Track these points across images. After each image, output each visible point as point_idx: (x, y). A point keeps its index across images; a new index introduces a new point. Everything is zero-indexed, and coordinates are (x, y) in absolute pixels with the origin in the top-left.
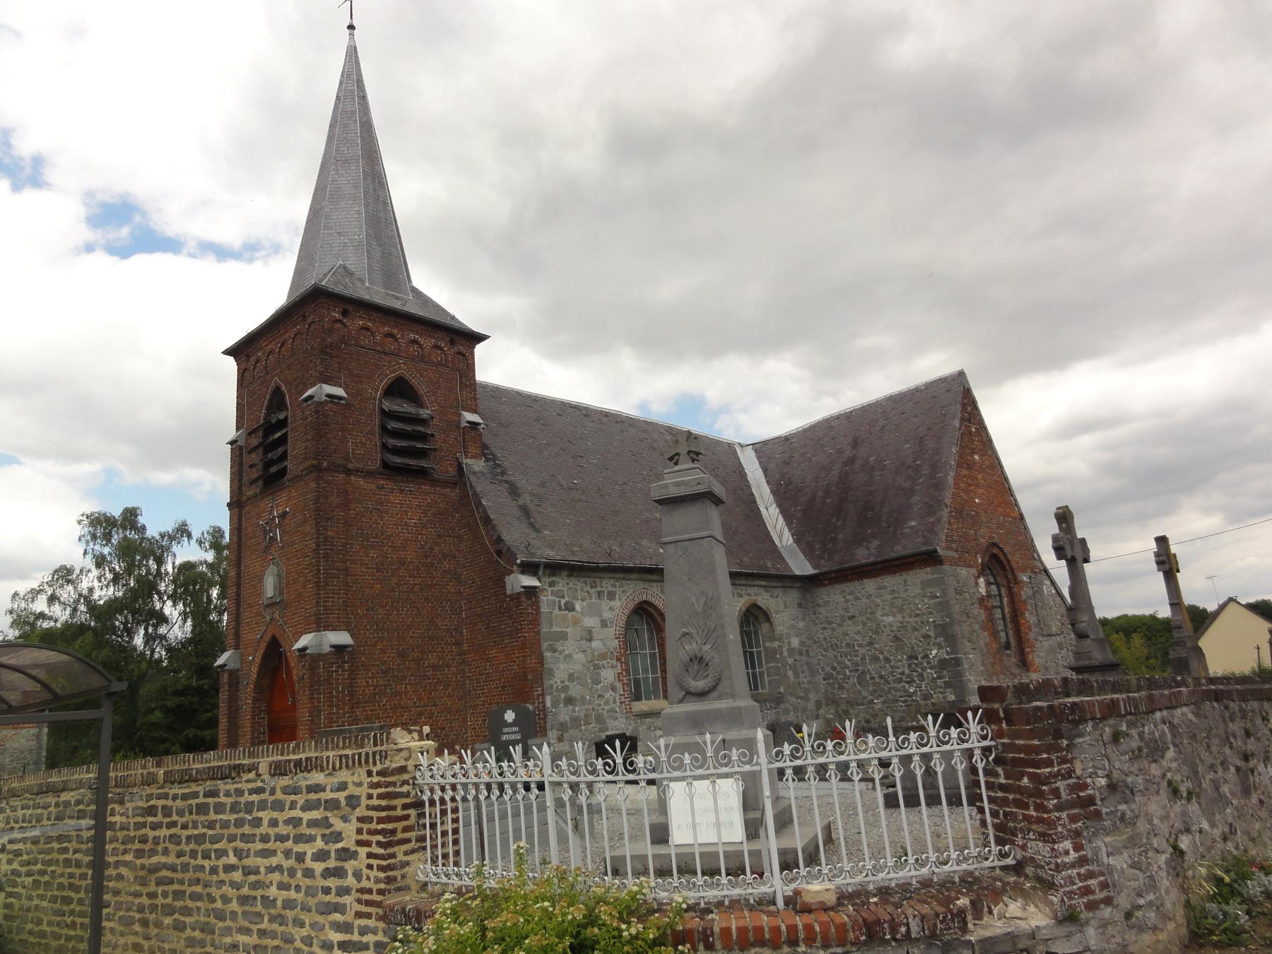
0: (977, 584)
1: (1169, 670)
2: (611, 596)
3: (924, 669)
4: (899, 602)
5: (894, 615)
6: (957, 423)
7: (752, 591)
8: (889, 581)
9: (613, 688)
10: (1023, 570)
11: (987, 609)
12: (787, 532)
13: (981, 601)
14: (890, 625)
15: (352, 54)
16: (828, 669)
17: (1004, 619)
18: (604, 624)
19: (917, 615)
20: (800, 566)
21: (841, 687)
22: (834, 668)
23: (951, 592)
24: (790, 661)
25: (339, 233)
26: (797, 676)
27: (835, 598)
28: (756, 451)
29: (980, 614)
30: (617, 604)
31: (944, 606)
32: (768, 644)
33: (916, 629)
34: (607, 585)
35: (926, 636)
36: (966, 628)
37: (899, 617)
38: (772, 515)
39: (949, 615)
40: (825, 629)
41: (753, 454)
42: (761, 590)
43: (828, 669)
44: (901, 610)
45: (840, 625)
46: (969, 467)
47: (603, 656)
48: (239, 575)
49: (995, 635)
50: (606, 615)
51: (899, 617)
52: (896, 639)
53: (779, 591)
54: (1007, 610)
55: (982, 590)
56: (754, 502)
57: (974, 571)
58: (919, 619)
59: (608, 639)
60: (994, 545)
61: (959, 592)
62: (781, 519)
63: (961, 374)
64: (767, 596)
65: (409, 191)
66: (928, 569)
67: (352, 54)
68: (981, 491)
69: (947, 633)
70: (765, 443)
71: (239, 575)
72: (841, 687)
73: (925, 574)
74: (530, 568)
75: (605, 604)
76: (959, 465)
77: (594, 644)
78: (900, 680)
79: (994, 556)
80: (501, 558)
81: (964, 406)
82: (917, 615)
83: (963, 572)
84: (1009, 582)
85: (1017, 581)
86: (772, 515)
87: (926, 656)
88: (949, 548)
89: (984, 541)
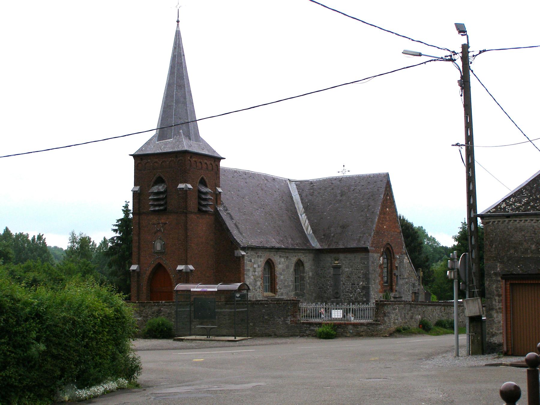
0: (380, 259)
1: (13, 331)
2: (261, 257)
3: (357, 289)
4: (351, 264)
5: (349, 268)
6: (382, 196)
7: (299, 254)
8: (349, 256)
9: (259, 288)
10: (398, 254)
11: (382, 269)
12: (309, 228)
13: (381, 266)
14: (347, 272)
15: (178, 35)
16: (321, 285)
17: (387, 272)
18: (259, 267)
19: (357, 269)
20: (315, 244)
21: (325, 292)
22: (323, 285)
23: (370, 263)
24: (308, 281)
25: (180, 118)
26: (310, 287)
27: (329, 260)
28: (297, 185)
29: (379, 270)
30: (262, 259)
31: (367, 267)
32: (301, 274)
33: (356, 274)
34: (260, 253)
35: (359, 277)
36: (373, 276)
37: (351, 269)
38: (303, 218)
39: (368, 271)
40: (322, 270)
41: (295, 186)
42: (302, 254)
43: (321, 285)
44: (352, 267)
45: (328, 269)
46: (384, 214)
47: (258, 277)
48: (139, 239)
49: (382, 278)
50: (260, 263)
51: (351, 269)
52: (348, 277)
53: (307, 254)
54: (389, 269)
55: (381, 262)
56: (297, 212)
57: (379, 255)
58: (358, 271)
59: (259, 271)
60: (388, 244)
61: (373, 263)
62: (307, 221)
63: (388, 175)
64: (303, 256)
65: (202, 102)
66: (364, 254)
67: (178, 35)
68: (387, 223)
69: (366, 277)
70: (301, 182)
71: (139, 239)
72: (325, 292)
73: (362, 255)
74: (244, 249)
75: (259, 259)
76: (380, 214)
77: (256, 273)
78: (348, 292)
79: (388, 249)
80: (233, 245)
81: (386, 188)
82: (357, 269)
83: (376, 255)
84: (391, 258)
85: (394, 258)
86: (303, 218)
87: (358, 284)
88: (372, 246)
89: (384, 243)
